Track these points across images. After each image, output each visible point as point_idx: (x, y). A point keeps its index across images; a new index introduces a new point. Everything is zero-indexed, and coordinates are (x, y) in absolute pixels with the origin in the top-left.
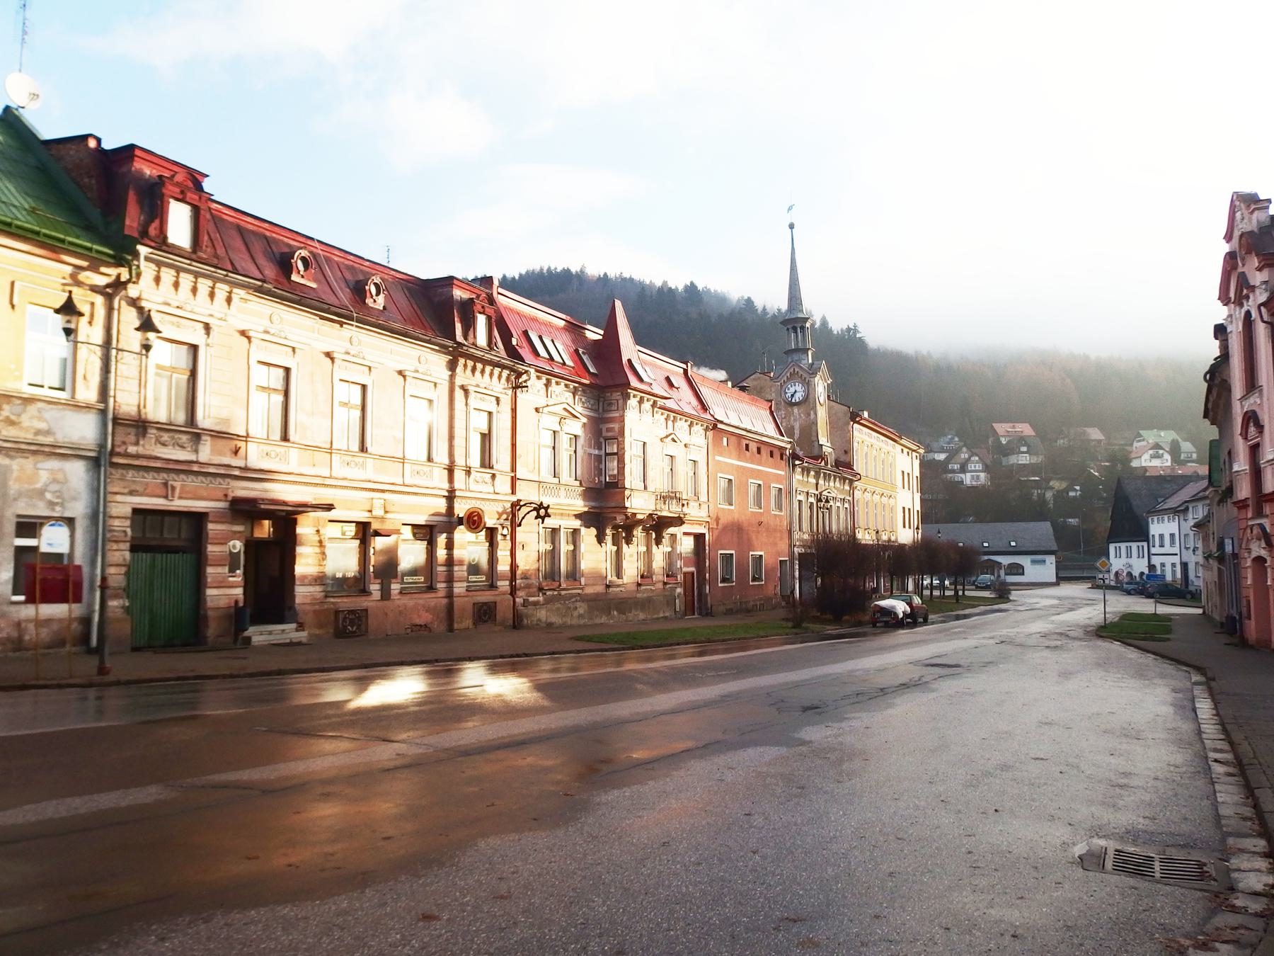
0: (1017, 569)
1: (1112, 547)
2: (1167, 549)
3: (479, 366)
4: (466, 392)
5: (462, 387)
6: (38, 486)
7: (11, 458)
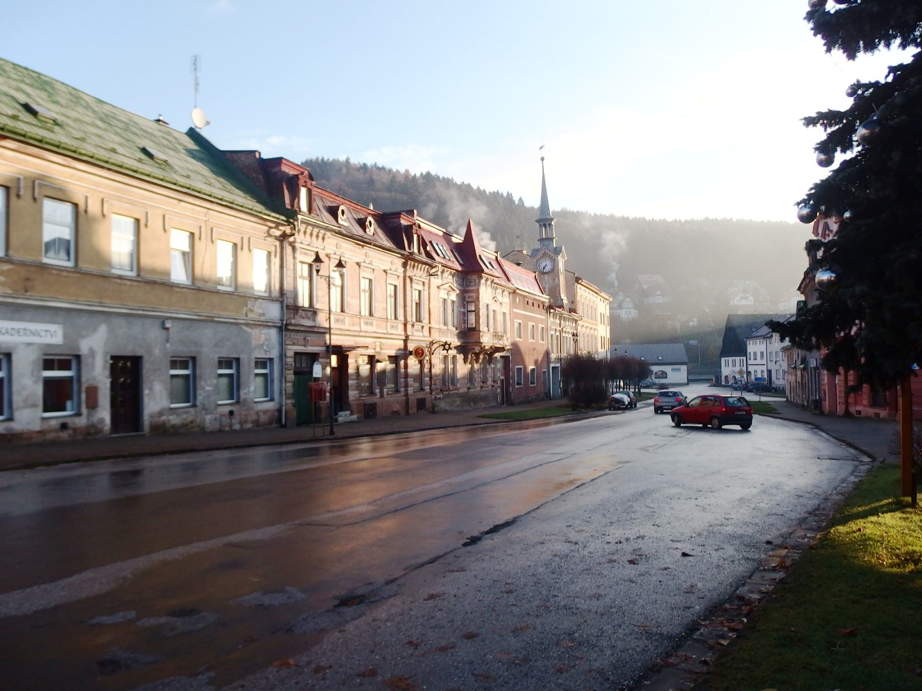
0: (664, 375)
1: (723, 360)
2: (759, 361)
3: (416, 264)
4: (411, 279)
5: (409, 277)
6: (261, 342)
7: (252, 328)
